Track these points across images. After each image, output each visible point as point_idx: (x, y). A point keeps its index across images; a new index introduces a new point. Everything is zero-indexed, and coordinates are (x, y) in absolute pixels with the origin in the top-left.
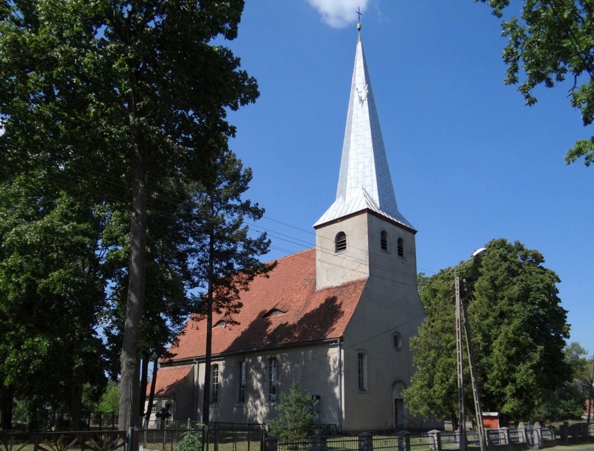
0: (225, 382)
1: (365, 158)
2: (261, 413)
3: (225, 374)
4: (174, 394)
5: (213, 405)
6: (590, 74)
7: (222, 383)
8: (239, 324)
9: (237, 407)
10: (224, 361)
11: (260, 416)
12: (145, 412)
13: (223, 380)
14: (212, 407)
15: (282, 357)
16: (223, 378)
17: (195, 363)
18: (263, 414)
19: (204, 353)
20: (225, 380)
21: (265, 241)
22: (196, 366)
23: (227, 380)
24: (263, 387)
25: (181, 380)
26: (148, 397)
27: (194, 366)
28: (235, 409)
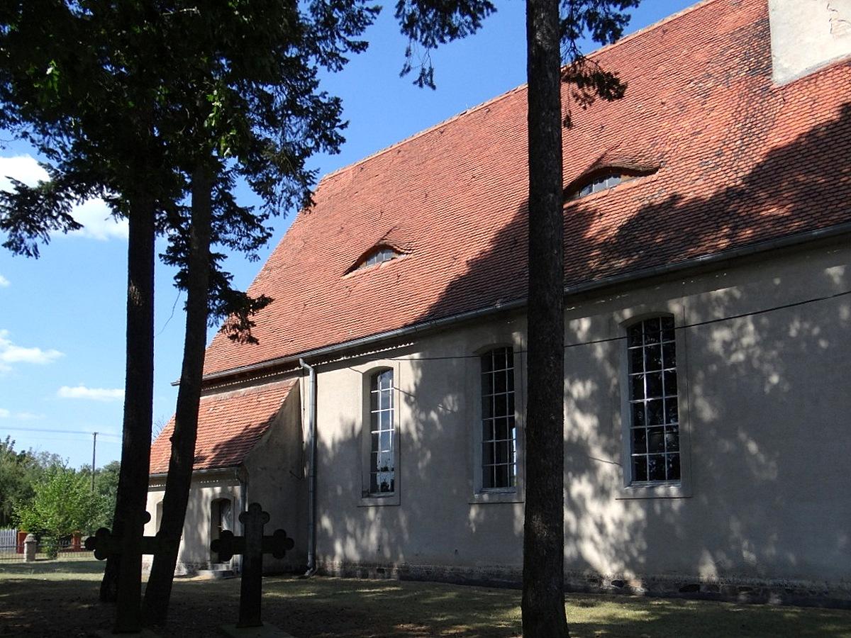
0: (428, 425)
1: (95, 434)
2: (601, 527)
3: (419, 399)
4: (239, 465)
5: (381, 501)
6: (431, 79)
7: (412, 428)
8: (402, 75)
9: (482, 504)
10: (416, 356)
11: (597, 538)
12: (151, 530)
13: (417, 419)
14: (377, 506)
15: (703, 308)
16: (413, 412)
17: (304, 373)
18: (610, 528)
19: (319, 375)
20: (423, 416)
21: (427, 72)
22: (306, 382)
23: (434, 416)
24: (604, 428)
25: (263, 425)
26: (158, 480)
27: (298, 380)
28: (473, 512)
